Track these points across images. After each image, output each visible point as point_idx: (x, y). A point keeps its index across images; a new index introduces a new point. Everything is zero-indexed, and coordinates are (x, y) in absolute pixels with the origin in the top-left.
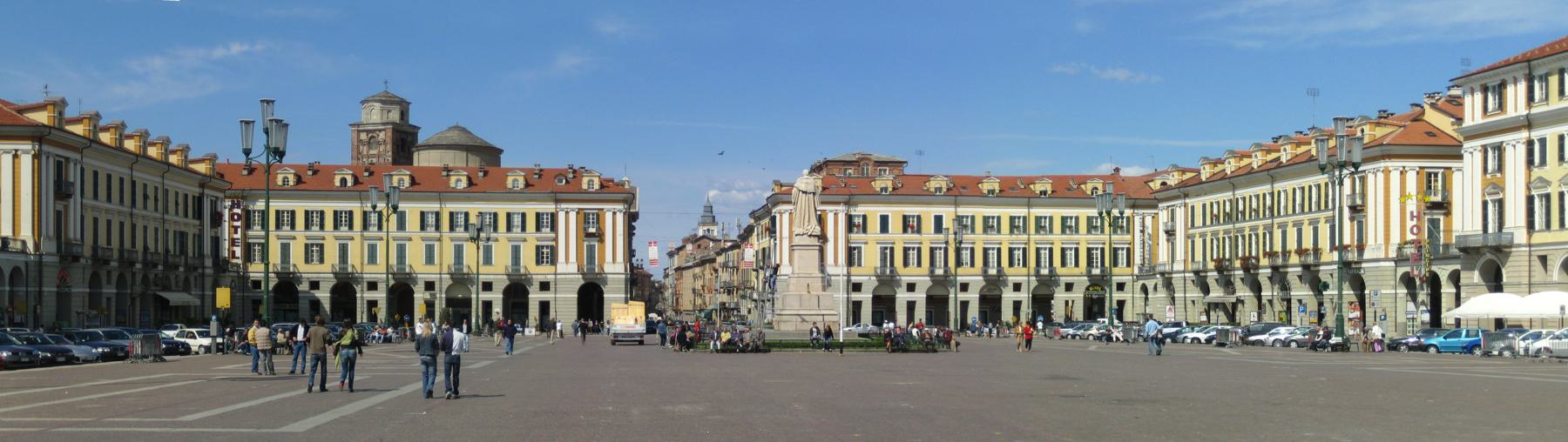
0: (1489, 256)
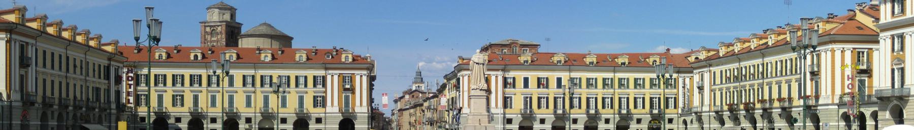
0: (895, 102)
